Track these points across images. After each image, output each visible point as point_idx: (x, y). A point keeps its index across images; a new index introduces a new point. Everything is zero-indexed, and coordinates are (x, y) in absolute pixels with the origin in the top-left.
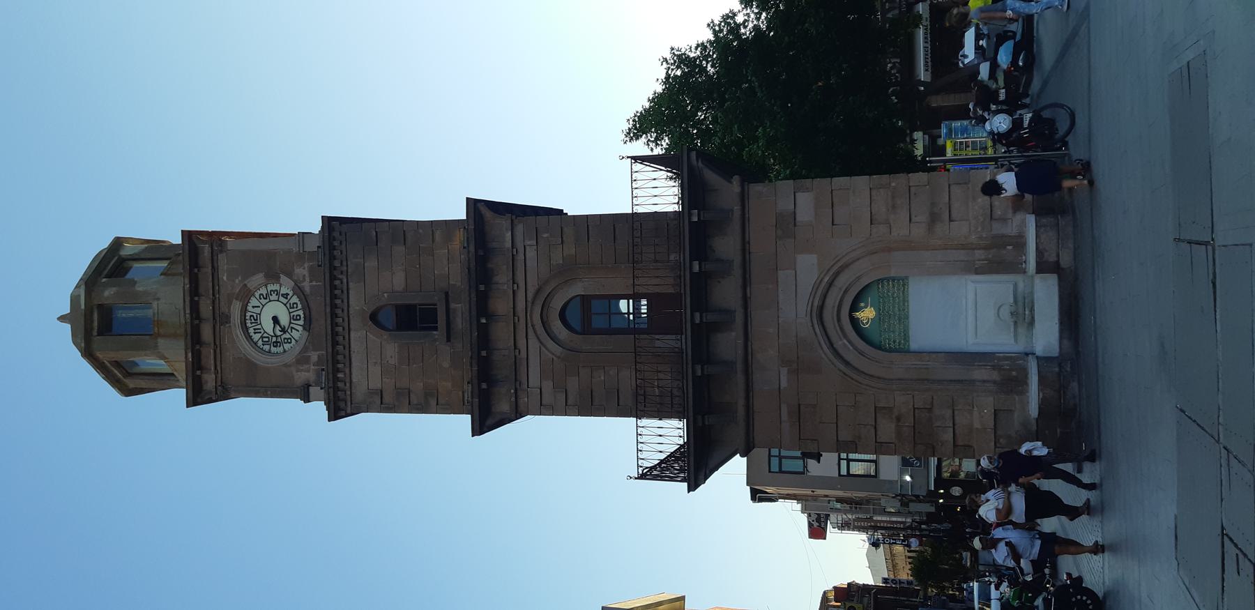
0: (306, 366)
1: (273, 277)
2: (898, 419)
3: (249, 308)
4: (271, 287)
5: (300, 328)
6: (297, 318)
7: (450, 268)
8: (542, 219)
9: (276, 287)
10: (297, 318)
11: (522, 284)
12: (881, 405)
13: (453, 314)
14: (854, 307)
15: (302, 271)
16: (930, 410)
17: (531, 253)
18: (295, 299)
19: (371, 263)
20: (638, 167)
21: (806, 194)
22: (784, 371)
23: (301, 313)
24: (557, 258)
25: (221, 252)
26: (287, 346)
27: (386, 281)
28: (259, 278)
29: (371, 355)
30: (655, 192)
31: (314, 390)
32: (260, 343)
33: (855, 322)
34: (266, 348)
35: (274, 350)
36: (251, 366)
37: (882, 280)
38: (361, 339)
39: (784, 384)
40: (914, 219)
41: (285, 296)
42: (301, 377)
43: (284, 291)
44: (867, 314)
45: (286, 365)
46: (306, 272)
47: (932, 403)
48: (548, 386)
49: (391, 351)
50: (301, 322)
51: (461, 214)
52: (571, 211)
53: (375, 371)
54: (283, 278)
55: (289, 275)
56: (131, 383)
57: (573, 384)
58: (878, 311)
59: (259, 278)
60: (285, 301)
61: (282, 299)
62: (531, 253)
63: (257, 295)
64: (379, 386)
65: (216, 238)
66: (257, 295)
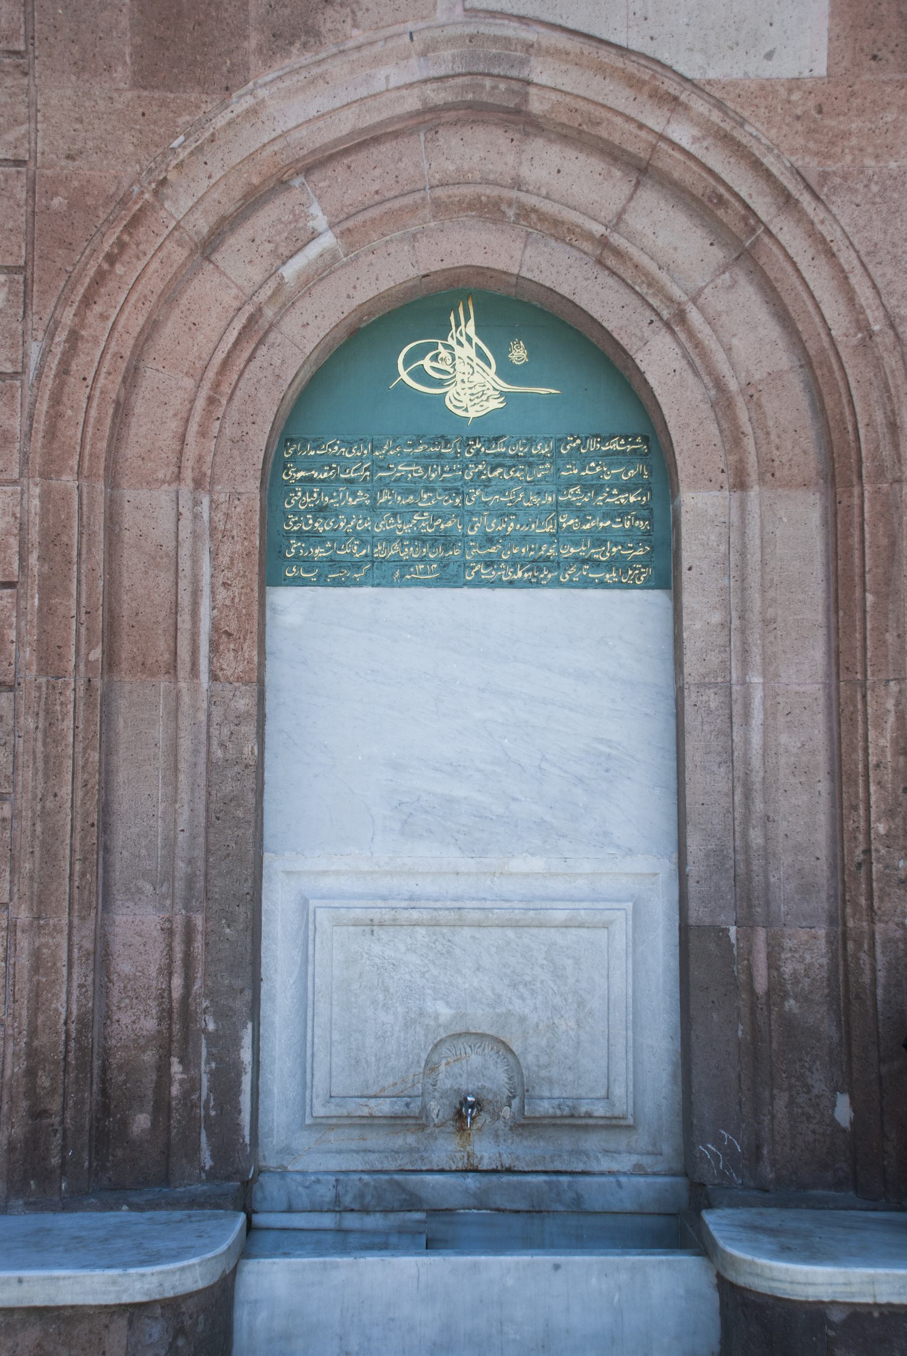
33: (421, 311)
44: (468, 377)
58: (487, 431)
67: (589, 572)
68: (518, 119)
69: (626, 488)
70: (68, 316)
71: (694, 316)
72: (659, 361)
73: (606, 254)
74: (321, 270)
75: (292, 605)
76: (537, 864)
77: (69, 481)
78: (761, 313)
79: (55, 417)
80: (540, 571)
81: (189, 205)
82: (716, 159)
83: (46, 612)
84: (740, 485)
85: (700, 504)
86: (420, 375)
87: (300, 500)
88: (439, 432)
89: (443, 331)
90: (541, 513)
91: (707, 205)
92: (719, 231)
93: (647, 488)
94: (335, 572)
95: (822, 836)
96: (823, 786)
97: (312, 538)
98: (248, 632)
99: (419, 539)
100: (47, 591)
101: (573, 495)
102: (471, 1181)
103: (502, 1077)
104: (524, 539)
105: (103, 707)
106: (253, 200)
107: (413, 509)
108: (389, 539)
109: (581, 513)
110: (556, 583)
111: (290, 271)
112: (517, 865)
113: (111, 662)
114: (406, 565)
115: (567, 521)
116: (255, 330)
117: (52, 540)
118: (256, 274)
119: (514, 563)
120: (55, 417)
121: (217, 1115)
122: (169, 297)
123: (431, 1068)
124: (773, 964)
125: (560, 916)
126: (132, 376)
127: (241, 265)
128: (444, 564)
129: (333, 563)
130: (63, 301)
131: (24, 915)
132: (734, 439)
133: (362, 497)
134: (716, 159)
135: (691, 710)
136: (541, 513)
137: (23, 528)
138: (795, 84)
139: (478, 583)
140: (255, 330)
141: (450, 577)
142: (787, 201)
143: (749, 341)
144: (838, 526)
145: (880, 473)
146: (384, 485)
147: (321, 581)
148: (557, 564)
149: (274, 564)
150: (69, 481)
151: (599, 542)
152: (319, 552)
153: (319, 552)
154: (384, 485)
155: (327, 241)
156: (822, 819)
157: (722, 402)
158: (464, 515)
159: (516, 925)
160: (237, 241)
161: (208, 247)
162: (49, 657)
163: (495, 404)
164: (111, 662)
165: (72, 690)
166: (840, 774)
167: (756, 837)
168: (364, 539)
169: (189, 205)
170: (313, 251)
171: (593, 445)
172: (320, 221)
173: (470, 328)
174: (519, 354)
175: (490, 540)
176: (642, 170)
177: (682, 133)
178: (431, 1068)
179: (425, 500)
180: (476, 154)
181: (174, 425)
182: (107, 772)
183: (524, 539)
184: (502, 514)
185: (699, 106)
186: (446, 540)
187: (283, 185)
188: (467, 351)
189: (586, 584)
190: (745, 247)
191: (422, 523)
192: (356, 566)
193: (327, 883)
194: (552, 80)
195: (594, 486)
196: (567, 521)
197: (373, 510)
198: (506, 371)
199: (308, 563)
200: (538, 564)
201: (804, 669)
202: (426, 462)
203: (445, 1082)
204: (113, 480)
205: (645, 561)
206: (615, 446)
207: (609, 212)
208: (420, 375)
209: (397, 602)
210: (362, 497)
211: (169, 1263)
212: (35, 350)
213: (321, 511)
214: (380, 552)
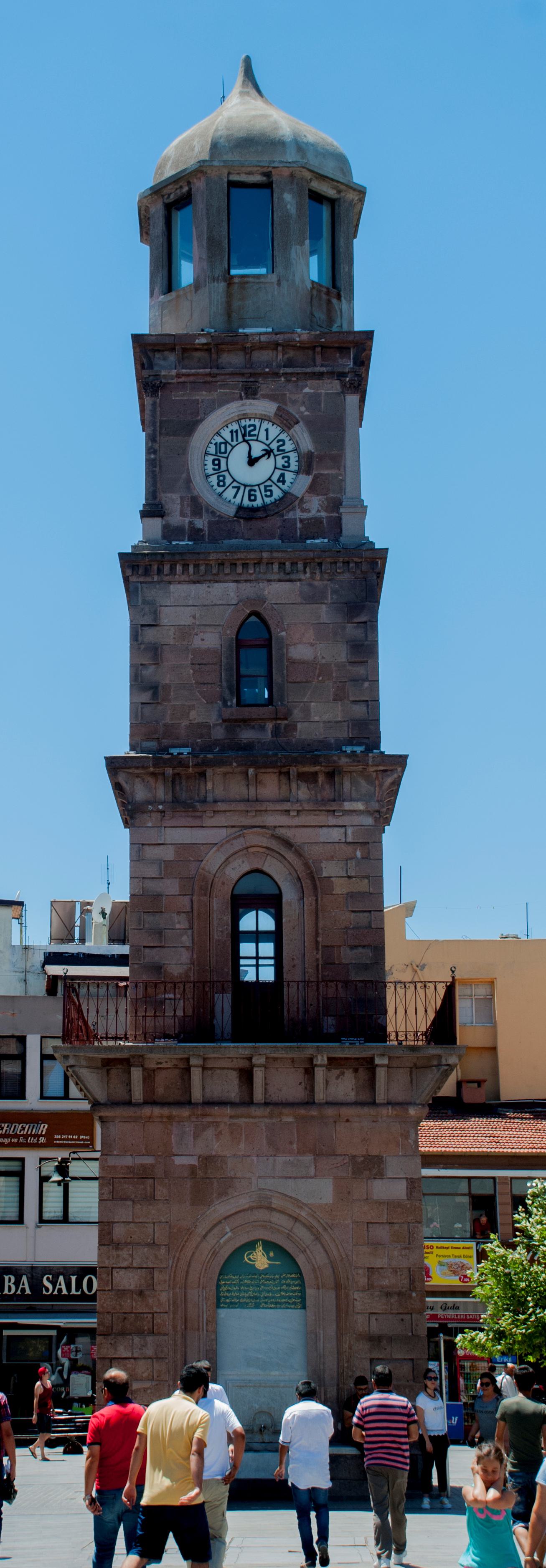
0: (188, 511)
1: (307, 463)
2: (141, 1293)
3: (265, 425)
4: (293, 457)
5: (238, 500)
6: (252, 497)
7: (318, 717)
8: (358, 415)
9: (294, 466)
10: (252, 497)
11: (297, 821)
12: (156, 1274)
13: (255, 680)
14: (268, 1246)
15: (315, 507)
16: (152, 1332)
17: (336, 835)
18: (277, 493)
19: (324, 613)
20: (442, 991)
21: (404, 1192)
22: (193, 1161)
23: (259, 503)
24: (329, 869)
25: (343, 385)
26: (214, 480)
27: (306, 640)
28: (307, 444)
29: (204, 608)
30: (411, 1012)
31: (157, 524)
32: (218, 440)
33: (251, 1246)
34: (212, 449)
35: (210, 459)
36: (189, 428)
37: (301, 1278)
38: (224, 596)
39: (178, 1161)
40: (373, 1318)
41: (282, 479)
42: (173, 502)
43: (289, 477)
44: (260, 1260)
45: (189, 481)
46: (313, 513)
47: (159, 1334)
48: (168, 854)
49: (210, 641)
50: (246, 503)
51: (388, 747)
52: (390, 838)
53: (184, 616)
54: (306, 481)
55: (313, 489)
56: (157, 209)
57: (170, 887)
58: (265, 1272)
59: (307, 444)
60: (275, 478)
61: (278, 473)
62: (336, 835)
63: (283, 436)
64: (165, 621)
65: (357, 384)
66: (283, 436)
67: (287, 1305)
68: (271, 1209)
69: (296, 1286)
70: (177, 1255)
71: (308, 1251)
72: (301, 1260)
73: (289, 1237)
74: (228, 1240)
75: (223, 1313)
76: (277, 1373)
77: (178, 1290)
78: (322, 1251)
79: (175, 1276)
80: (277, 1305)
81: (201, 1230)
82: (311, 1219)
83: (174, 1318)
84: (318, 1288)
85: (310, 1292)
86: (249, 1259)
87: (224, 1288)
88: (252, 1271)
89: (255, 1249)
90: (277, 1292)
91: (310, 1228)
92: (312, 1233)
93: (300, 1285)
94: (232, 1305)
95: (335, 1367)
96: (336, 1356)
97: (226, 1297)
98: (213, 1321)
99: (250, 1297)
100: (174, 1313)
101: (284, 1287)
102: (263, 1445)
103: (269, 1421)
104: (273, 1297)
105: (184, 1337)
106: (215, 1226)
107: (249, 1291)
108: (243, 1297)
109: (286, 1292)
110: (280, 1308)
111: (222, 1241)
112: (273, 1373)
113: (186, 1328)
114: (247, 1304)
115: (283, 1293)
116: (215, 1254)
117: (174, 1303)
118: (215, 1242)
119: (271, 1303)
120: (175, 1276)
121: (488, 1220)
122: (197, 1247)
123: (254, 1419)
124: (325, 1394)
125: (282, 1385)
126: (189, 1266)
127: (211, 1240)
128: (255, 1303)
129: (231, 1303)
130: (176, 1251)
131: (171, 1383)
132: (317, 1278)
133: (237, 1288)
134: (311, 1219)
135: (311, 1337)
136: (277, 1292)
137: (169, 1301)
138: (326, 1204)
139: (263, 1308)
140: (215, 1254)
141: (257, 1306)
142: (325, 1229)
143: (320, 1258)
144: (338, 1297)
145: (345, 1288)
146: (242, 1285)
147: (228, 1307)
148: (281, 1303)
149: (218, 1307)
150: (178, 1290)
151: (290, 1298)
152: (228, 1301)
153: (228, 1301)
154: (242, 1285)
155: (229, 1234)
156: (335, 1363)
157: (314, 1270)
158: (260, 1292)
159: (272, 1387)
160: (210, 1235)
161: (205, 1236)
162: (174, 1328)
163: (267, 1266)
164: (186, 1328)
165: (179, 1335)
166: (339, 1353)
167: (322, 1367)
168: (238, 1298)
169: (201, 1230)
170: (226, 1237)
171: (289, 1276)
172: (228, 1230)
173: (261, 1248)
174: (272, 1254)
175: (266, 1298)
176: (296, 1219)
177: (303, 1214)
178: (254, 1419)
179: (251, 1288)
180: (261, 1215)
181: (198, 1275)
182: (186, 1353)
183: (273, 1297)
184: (268, 1292)
185: (307, 1209)
186: (256, 1298)
187: (220, 1222)
188: (260, 1254)
189: (287, 1308)
190: (317, 1238)
191: (250, 1294)
192: (236, 1304)
193: (231, 1377)
194: (276, 1202)
195: (288, 1285)
196: (283, 1293)
197: (240, 1291)
198: (269, 1258)
199: (225, 1303)
200: (276, 1303)
201: (332, 1330)
202: (251, 1279)
203: (257, 1422)
204: (185, 1288)
205: (300, 1303)
206: (293, 1276)
207: (289, 1228)
208: (249, 1259)
209: (246, 1312)
210: (237, 1288)
211: (439, 1168)
212: (171, 1262)
213: (228, 1291)
214: (242, 1301)
